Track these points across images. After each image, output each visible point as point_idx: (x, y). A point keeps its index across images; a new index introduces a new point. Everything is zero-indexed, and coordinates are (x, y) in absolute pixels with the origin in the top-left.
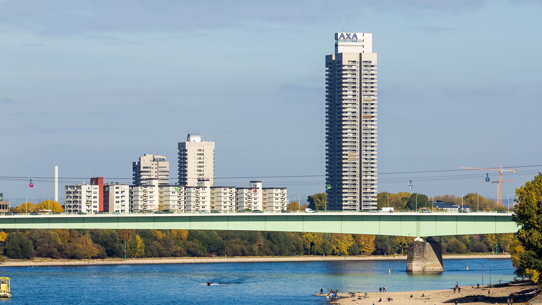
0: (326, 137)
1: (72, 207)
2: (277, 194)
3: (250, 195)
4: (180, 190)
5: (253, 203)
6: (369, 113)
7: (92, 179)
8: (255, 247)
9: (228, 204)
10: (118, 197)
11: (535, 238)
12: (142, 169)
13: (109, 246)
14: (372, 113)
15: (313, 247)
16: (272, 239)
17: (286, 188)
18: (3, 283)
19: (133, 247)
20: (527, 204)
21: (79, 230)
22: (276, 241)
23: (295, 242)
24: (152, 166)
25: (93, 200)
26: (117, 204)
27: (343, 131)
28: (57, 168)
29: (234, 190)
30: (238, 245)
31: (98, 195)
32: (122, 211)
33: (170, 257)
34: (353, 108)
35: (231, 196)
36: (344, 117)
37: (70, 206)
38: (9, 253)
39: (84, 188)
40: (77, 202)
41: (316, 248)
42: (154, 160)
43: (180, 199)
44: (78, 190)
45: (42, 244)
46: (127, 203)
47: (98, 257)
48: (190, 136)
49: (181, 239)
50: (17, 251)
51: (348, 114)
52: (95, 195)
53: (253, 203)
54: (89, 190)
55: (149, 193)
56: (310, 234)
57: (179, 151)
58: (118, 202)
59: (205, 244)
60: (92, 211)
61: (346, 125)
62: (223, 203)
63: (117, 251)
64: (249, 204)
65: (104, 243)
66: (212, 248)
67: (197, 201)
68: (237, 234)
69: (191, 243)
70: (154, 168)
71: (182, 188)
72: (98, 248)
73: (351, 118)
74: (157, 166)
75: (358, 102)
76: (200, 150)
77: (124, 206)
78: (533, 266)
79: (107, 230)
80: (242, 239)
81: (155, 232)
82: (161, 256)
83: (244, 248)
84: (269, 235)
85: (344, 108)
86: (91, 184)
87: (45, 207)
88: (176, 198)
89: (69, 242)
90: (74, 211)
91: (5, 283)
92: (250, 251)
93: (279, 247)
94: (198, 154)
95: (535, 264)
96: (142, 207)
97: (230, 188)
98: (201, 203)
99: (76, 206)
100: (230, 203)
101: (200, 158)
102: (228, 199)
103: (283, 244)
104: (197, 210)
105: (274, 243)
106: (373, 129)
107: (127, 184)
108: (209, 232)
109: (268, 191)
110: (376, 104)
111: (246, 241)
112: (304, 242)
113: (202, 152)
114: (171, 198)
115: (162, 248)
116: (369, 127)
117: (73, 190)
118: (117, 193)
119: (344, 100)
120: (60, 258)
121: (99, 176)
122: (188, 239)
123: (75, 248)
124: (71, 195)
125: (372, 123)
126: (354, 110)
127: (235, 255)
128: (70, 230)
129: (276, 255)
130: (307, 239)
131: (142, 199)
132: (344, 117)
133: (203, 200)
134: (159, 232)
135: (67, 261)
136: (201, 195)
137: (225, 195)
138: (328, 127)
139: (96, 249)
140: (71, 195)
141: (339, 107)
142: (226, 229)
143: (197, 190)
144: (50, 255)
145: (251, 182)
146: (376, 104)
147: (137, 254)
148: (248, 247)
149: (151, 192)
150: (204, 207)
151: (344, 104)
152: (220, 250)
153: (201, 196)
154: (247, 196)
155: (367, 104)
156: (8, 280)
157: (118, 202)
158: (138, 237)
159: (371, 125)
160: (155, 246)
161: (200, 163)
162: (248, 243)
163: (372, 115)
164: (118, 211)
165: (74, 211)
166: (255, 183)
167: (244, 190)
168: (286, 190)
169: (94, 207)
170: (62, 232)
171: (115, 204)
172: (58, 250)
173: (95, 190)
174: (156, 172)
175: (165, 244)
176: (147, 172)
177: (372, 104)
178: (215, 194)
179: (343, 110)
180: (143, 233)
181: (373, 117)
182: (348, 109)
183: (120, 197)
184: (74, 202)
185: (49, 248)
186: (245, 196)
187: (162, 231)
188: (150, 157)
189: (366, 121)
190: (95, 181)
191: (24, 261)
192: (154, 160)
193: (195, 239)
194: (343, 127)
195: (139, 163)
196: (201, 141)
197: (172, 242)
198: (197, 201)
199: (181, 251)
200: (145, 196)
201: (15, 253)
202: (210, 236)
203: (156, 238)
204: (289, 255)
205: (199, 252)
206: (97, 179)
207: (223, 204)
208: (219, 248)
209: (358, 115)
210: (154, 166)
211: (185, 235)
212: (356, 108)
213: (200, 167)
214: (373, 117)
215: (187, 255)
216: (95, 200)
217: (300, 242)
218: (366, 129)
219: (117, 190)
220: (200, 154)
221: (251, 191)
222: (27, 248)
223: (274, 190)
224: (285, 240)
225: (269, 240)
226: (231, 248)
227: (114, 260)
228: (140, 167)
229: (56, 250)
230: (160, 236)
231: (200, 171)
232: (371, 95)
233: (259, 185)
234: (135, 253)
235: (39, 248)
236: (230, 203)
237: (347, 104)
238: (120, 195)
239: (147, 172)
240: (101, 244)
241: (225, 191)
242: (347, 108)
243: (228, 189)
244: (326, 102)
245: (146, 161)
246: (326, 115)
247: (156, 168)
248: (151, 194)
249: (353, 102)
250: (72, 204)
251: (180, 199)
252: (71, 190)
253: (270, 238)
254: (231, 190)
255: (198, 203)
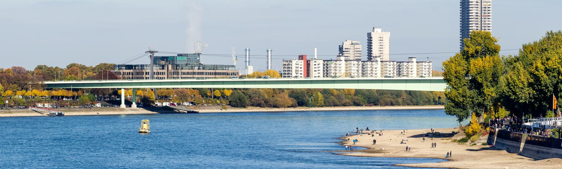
0: (460, 29)
1: (287, 74)
2: (425, 66)
3: (408, 66)
4: (358, 63)
5: (410, 72)
6: (487, 13)
7: (299, 56)
8: (400, 100)
9: (392, 72)
10: (316, 68)
11: (454, 95)
12: (344, 50)
13: (300, 99)
14: (489, 13)
15: (440, 99)
16: (412, 94)
17: (431, 62)
18: (144, 123)
19: (316, 100)
20: (448, 72)
21: (279, 89)
22: (414, 96)
23: (427, 96)
24: (350, 48)
25: (300, 69)
26: (315, 72)
27: (470, 25)
28: (316, 49)
29: (395, 63)
30: (389, 99)
31: (303, 66)
32: (318, 76)
33: (341, 106)
34: (477, 10)
35: (394, 67)
36: (470, 16)
37: (285, 74)
38: (232, 104)
39: (294, 62)
40: (290, 71)
41: (442, 100)
42: (352, 44)
43: (358, 69)
44: (290, 63)
45: (254, 98)
46: (321, 72)
47: (292, 106)
48: (375, 29)
49: (350, 95)
50: (237, 103)
51: (473, 14)
52: (301, 66)
53: (410, 72)
54: (297, 63)
55: (338, 65)
56: (335, 90)
57: (368, 38)
58: (316, 71)
59: (366, 98)
60: (299, 77)
61: (472, 21)
62: (388, 71)
63: (305, 103)
64: (408, 72)
65: (296, 98)
66: (371, 100)
67: (372, 70)
68: (388, 92)
69: (356, 97)
70: (352, 49)
71: (360, 62)
72: (292, 100)
73: (475, 16)
74: (353, 48)
75: (479, 7)
76: (381, 38)
77: (320, 73)
78: (453, 113)
79: (299, 89)
80: (392, 95)
81: (332, 90)
82: (335, 105)
83: (393, 100)
84: (410, 93)
85: (471, 10)
86: (299, 59)
87: (268, 74)
88: (356, 69)
89: (273, 96)
90: (288, 77)
91: (146, 123)
92: (396, 102)
93: (416, 100)
94: (379, 40)
95: (454, 112)
96: (334, 74)
97: (393, 62)
98: (374, 71)
99: (289, 74)
100: (393, 72)
101: (381, 43)
102: (392, 69)
103: (419, 98)
104: (372, 76)
105: (413, 97)
106: (489, 24)
107: (322, 60)
108: (369, 91)
109: (420, 64)
110: (491, 8)
111: (394, 96)
112: (433, 96)
113: (382, 39)
114: (352, 68)
115: (336, 100)
116: (487, 22)
117: (288, 63)
118: (315, 65)
119: (470, 5)
120: (266, 107)
121: (304, 54)
122: (355, 95)
123: (276, 101)
124: (286, 66)
125: (489, 20)
126: (477, 12)
127: (386, 104)
128: (274, 89)
129: (414, 105)
130: (436, 95)
131: (406, 70)
132: (470, 16)
133: (376, 69)
134: (335, 90)
135: (270, 109)
136: (374, 66)
137: (390, 67)
138: (461, 23)
139: (290, 101)
140: (286, 66)
141: (467, 9)
142: (381, 89)
143: (372, 63)
144: (259, 105)
145: (409, 58)
146: (491, 8)
147: (318, 105)
148: (395, 100)
149: (340, 65)
150: (376, 74)
151: (470, 7)
152: (376, 101)
153: (374, 67)
154: (406, 67)
155: (485, 8)
156: (148, 122)
157: (316, 71)
158: (319, 94)
159: (488, 21)
160: (332, 99)
161: (381, 45)
162: (396, 97)
163: (489, 15)
164: (316, 77)
165: (288, 77)
166: (411, 59)
167: (404, 63)
168: (431, 63)
169: (300, 74)
170: (268, 90)
171: (314, 72)
172: (265, 102)
173: (301, 63)
174: (353, 52)
175: (339, 98)
176: (348, 51)
177: (489, 8)
178: (384, 66)
179: (470, 12)
180: (325, 91)
181: (489, 16)
182: (473, 11)
183: (317, 68)
184: (288, 71)
185: (259, 100)
186: (405, 67)
187: (262, 89)
188: (349, 42)
189: (485, 18)
190: (301, 57)
191: (241, 109)
192: (352, 44)
193: (359, 95)
194: (470, 23)
195: (342, 46)
196: (382, 32)
197: (344, 96)
198: (372, 70)
199: (349, 102)
200: (408, 68)
201: (236, 104)
202: (370, 93)
203: (332, 94)
204: (423, 105)
205: (361, 103)
206: (302, 56)
207: (388, 72)
208: (376, 101)
209: (479, 15)
210: (352, 48)
211: (353, 92)
212: (478, 10)
213: (381, 48)
214: (489, 16)
215: (354, 105)
216: (301, 69)
217: (431, 97)
218: (485, 24)
219: (315, 63)
220: (381, 40)
221: (408, 64)
222: (243, 101)
223: (424, 63)
224: (421, 95)
225: (410, 95)
226: (384, 100)
227: (302, 109)
228: (343, 49)
229: (263, 102)
230: (336, 93)
231: (381, 51)
232: (488, 2)
233: (414, 60)
234: (318, 104)
235: (252, 100)
236: (393, 72)
237: (472, 7)
238: (317, 66)
239: (348, 51)
240: (295, 98)
241: (390, 64)
242: (472, 10)
243: (391, 62)
244: (460, 6)
245: (346, 45)
246: (460, 14)
247: (353, 49)
248: (340, 66)
249: (476, 6)
250: (286, 72)
251: (358, 69)
252: (286, 63)
253: (410, 94)
254: (393, 63)
255: (372, 72)
